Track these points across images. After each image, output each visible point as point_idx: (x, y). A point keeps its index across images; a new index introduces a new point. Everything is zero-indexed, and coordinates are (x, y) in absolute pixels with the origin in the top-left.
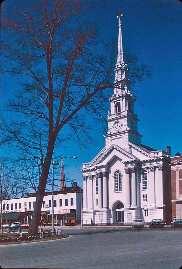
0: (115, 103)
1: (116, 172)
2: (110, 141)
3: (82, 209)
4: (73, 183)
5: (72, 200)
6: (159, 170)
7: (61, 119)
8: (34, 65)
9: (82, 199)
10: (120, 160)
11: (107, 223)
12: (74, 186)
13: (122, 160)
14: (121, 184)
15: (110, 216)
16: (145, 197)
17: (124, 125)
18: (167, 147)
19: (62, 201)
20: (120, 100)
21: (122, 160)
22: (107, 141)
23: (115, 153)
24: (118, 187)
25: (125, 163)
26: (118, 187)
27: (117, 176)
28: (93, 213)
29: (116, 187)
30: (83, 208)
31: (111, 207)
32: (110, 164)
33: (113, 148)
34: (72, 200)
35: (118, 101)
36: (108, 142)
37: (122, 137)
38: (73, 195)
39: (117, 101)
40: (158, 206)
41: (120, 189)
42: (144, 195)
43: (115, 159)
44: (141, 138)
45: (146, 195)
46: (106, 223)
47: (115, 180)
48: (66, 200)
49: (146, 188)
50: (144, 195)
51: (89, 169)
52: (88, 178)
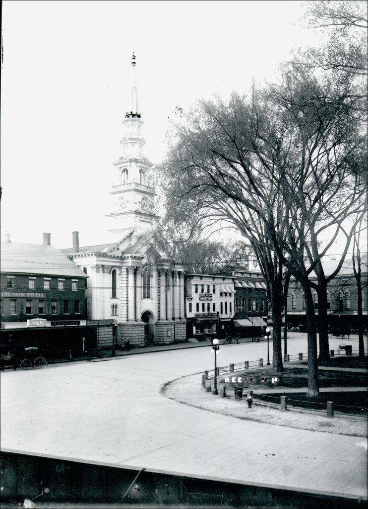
0: (122, 169)
35: (124, 168)
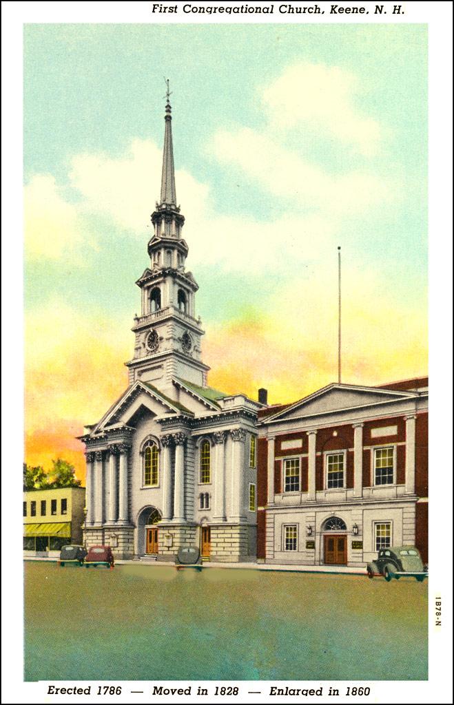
0: (152, 289)
1: (146, 444)
2: (136, 374)
4: (322, 537)
5: (64, 502)
10: (154, 415)
13: (156, 415)
14: (310, 548)
16: (336, 548)
17: (167, 339)
19: (66, 503)
20: (158, 283)
21: (156, 415)
23: (142, 400)
24: (151, 476)
25: (161, 422)
26: (151, 476)
29: (147, 477)
31: (136, 519)
32: (136, 422)
33: (138, 391)
34: (64, 502)
35: (155, 286)
36: (272, 549)
37: (159, 367)
39: (153, 285)
40: (230, 521)
43: (144, 413)
47: (145, 460)
48: (54, 502)
49: (207, 480)
51: (96, 438)
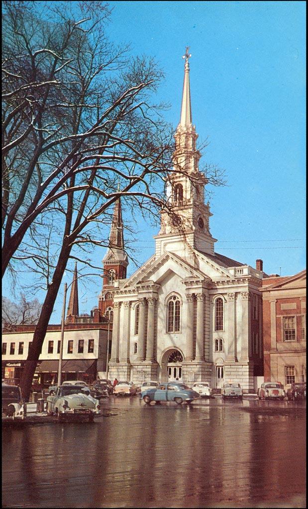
3: (109, 360)
5: (91, 342)
6: (243, 299)
7: (85, 214)
8: (47, 129)
9: (111, 342)
11: (249, 389)
12: (3, 96)
15: (156, 375)
18: (258, 261)
22: (158, 245)
24: (173, 324)
27: (173, 304)
28: (128, 369)
29: (169, 328)
30: (110, 358)
34: (91, 342)
35: (178, 183)
38: (95, 335)
41: (176, 328)
42: (217, 341)
44: (215, 243)
45: (221, 340)
46: (248, 388)
50: (217, 341)
52: (122, 304)
